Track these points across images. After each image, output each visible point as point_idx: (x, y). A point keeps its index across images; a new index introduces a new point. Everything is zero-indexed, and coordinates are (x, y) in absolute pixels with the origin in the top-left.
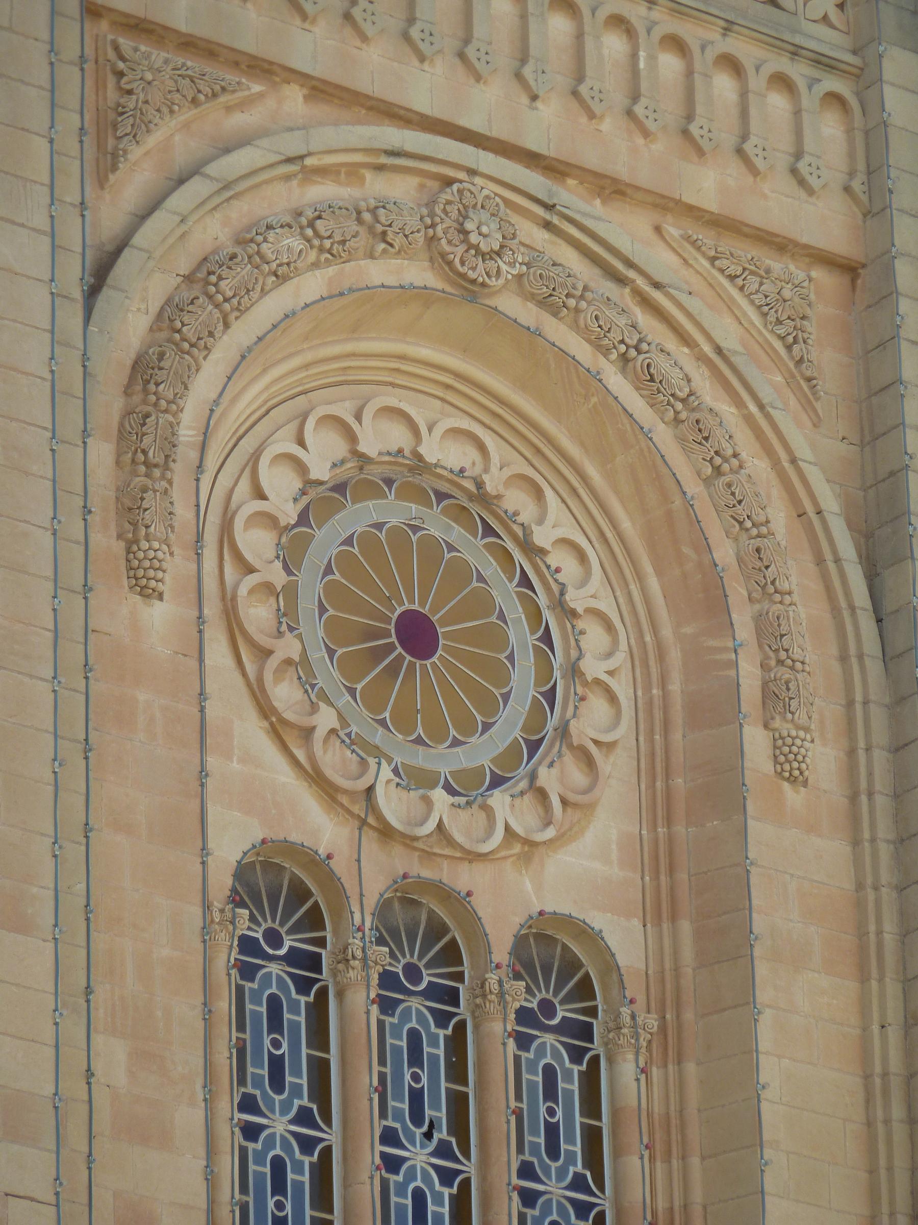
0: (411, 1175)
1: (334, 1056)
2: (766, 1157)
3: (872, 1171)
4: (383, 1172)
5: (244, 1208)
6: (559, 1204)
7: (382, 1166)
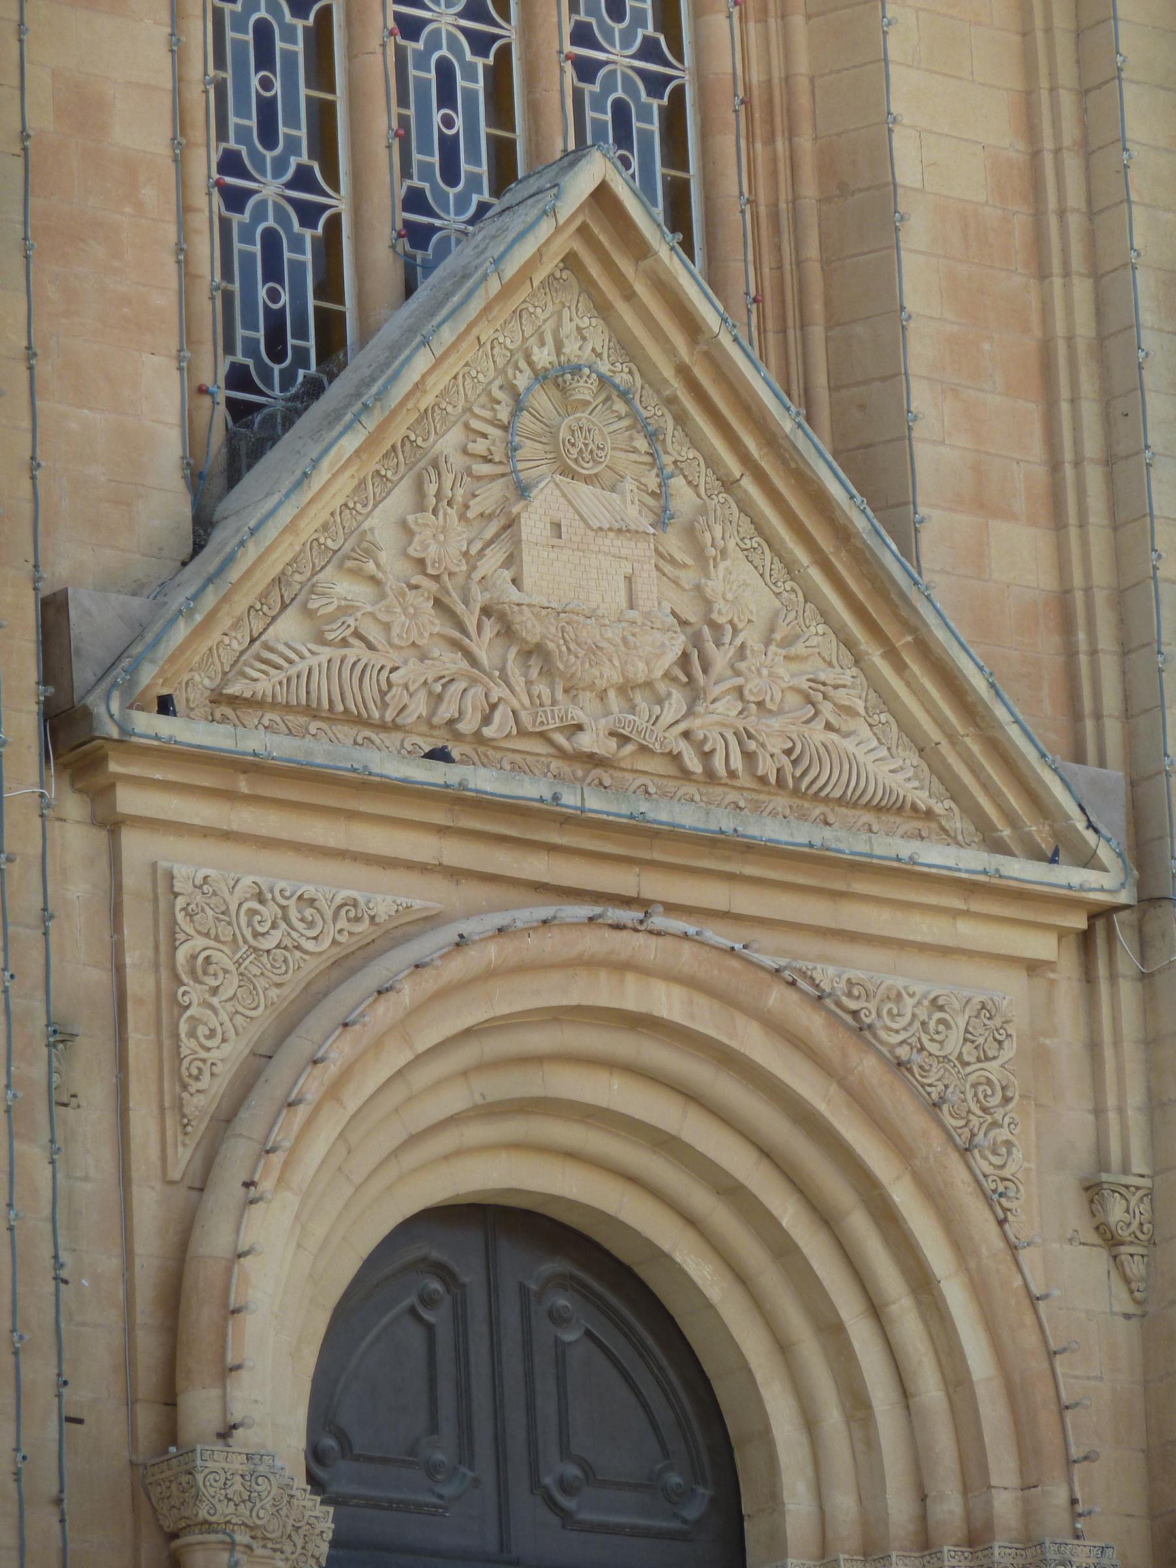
0: (434, 42)
1: (340, 98)
2: (888, 15)
3: (1026, 33)
4: (398, 38)
5: (220, 88)
6: (625, 77)
7: (397, 31)
